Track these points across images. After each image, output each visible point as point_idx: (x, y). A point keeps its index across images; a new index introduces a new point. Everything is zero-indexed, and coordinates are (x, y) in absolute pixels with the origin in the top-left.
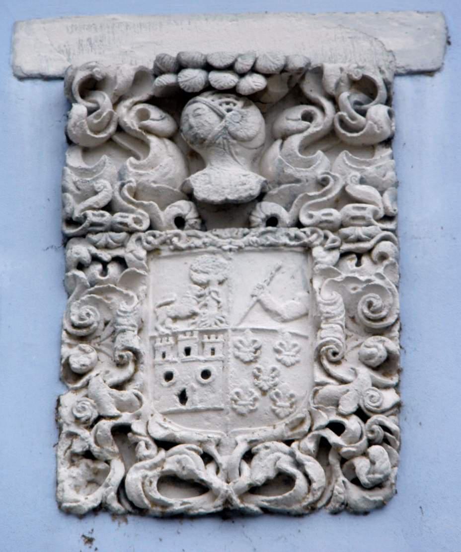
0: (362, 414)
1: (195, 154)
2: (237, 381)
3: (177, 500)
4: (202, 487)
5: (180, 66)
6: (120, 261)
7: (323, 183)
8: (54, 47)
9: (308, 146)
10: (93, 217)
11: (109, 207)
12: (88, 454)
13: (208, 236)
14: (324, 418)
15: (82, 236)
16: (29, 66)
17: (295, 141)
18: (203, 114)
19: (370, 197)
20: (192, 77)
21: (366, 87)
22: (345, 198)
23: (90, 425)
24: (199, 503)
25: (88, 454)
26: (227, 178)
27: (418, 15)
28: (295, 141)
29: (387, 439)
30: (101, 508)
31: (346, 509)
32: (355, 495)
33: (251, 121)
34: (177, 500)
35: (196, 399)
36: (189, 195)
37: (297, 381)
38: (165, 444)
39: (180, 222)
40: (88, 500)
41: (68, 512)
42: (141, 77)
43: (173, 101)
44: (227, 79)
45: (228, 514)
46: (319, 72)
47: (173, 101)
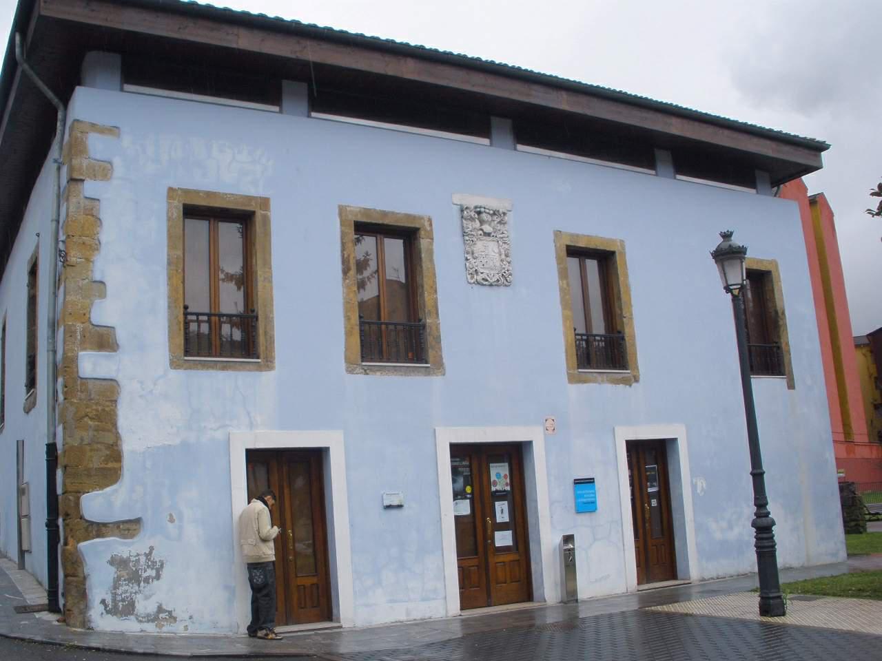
0: (508, 271)
1: (482, 222)
2: (491, 264)
3: (485, 283)
4: (487, 280)
5: (480, 207)
6: (472, 241)
7: (499, 230)
8: (458, 199)
9: (498, 223)
10: (469, 232)
11: (471, 231)
12: (471, 274)
13: (485, 238)
14: (503, 271)
15: (467, 235)
16: (455, 202)
17: (496, 222)
18: (484, 216)
19: (420, 295)
20: (482, 210)
21: (504, 214)
22: (503, 233)
23: (471, 269)
24: (486, 283)
25: (471, 274)
26: (487, 228)
27: (303, 610)
28: (496, 222)
29: (510, 275)
30: (474, 283)
31: (506, 286)
32: (507, 283)
33: (489, 218)
34: (485, 283)
35: (485, 266)
36: (482, 230)
37: (498, 264)
38: (482, 273)
39: (481, 235)
40: (472, 281)
41: (470, 283)
42: (476, 207)
43: (479, 213)
44: (487, 211)
45: (491, 285)
46: (498, 211)
47: (479, 213)
